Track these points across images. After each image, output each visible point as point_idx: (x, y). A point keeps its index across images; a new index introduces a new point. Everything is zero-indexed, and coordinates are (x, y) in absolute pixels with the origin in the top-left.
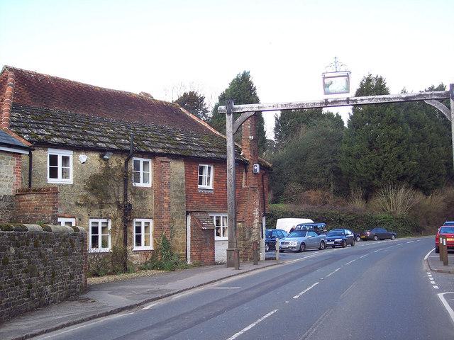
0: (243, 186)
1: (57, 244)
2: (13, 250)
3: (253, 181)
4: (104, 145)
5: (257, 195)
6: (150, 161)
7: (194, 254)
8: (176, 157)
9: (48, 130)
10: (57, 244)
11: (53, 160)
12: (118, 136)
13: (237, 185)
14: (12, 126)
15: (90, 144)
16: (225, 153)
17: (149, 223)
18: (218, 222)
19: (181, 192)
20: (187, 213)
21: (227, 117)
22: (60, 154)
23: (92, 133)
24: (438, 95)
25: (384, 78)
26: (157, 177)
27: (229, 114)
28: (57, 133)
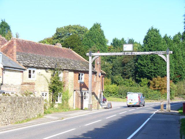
0: (95, 81)
1: (37, 100)
2: (28, 102)
3: (99, 79)
4: (46, 67)
5: (100, 83)
6: (83, 74)
7: (76, 105)
8: (70, 71)
9: (28, 61)
10: (37, 100)
11: (30, 72)
12: (51, 63)
13: (92, 81)
14: (17, 60)
15: (42, 66)
16: (88, 69)
17: (47, 94)
18: (85, 94)
19: (72, 83)
20: (74, 90)
21: (89, 57)
22: (32, 70)
23: (42, 62)
24: (163, 53)
25: (102, 25)
26: (85, 79)
27: (90, 56)
28: (31, 63)
